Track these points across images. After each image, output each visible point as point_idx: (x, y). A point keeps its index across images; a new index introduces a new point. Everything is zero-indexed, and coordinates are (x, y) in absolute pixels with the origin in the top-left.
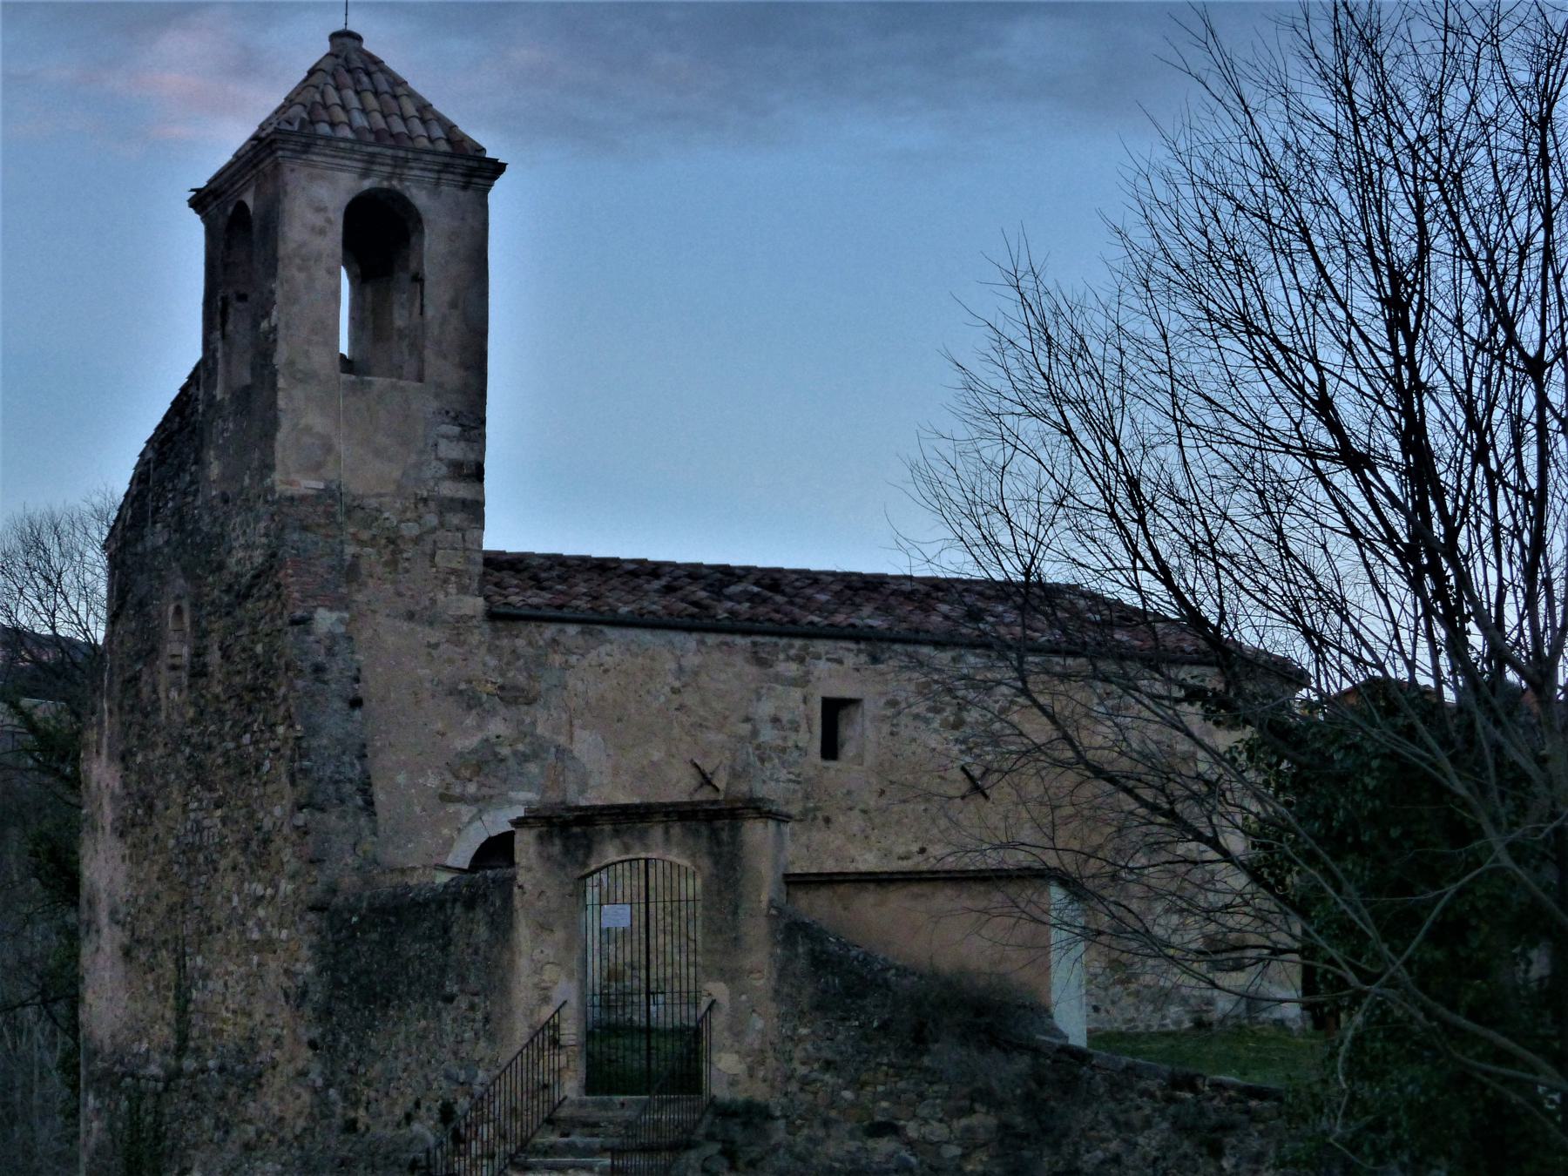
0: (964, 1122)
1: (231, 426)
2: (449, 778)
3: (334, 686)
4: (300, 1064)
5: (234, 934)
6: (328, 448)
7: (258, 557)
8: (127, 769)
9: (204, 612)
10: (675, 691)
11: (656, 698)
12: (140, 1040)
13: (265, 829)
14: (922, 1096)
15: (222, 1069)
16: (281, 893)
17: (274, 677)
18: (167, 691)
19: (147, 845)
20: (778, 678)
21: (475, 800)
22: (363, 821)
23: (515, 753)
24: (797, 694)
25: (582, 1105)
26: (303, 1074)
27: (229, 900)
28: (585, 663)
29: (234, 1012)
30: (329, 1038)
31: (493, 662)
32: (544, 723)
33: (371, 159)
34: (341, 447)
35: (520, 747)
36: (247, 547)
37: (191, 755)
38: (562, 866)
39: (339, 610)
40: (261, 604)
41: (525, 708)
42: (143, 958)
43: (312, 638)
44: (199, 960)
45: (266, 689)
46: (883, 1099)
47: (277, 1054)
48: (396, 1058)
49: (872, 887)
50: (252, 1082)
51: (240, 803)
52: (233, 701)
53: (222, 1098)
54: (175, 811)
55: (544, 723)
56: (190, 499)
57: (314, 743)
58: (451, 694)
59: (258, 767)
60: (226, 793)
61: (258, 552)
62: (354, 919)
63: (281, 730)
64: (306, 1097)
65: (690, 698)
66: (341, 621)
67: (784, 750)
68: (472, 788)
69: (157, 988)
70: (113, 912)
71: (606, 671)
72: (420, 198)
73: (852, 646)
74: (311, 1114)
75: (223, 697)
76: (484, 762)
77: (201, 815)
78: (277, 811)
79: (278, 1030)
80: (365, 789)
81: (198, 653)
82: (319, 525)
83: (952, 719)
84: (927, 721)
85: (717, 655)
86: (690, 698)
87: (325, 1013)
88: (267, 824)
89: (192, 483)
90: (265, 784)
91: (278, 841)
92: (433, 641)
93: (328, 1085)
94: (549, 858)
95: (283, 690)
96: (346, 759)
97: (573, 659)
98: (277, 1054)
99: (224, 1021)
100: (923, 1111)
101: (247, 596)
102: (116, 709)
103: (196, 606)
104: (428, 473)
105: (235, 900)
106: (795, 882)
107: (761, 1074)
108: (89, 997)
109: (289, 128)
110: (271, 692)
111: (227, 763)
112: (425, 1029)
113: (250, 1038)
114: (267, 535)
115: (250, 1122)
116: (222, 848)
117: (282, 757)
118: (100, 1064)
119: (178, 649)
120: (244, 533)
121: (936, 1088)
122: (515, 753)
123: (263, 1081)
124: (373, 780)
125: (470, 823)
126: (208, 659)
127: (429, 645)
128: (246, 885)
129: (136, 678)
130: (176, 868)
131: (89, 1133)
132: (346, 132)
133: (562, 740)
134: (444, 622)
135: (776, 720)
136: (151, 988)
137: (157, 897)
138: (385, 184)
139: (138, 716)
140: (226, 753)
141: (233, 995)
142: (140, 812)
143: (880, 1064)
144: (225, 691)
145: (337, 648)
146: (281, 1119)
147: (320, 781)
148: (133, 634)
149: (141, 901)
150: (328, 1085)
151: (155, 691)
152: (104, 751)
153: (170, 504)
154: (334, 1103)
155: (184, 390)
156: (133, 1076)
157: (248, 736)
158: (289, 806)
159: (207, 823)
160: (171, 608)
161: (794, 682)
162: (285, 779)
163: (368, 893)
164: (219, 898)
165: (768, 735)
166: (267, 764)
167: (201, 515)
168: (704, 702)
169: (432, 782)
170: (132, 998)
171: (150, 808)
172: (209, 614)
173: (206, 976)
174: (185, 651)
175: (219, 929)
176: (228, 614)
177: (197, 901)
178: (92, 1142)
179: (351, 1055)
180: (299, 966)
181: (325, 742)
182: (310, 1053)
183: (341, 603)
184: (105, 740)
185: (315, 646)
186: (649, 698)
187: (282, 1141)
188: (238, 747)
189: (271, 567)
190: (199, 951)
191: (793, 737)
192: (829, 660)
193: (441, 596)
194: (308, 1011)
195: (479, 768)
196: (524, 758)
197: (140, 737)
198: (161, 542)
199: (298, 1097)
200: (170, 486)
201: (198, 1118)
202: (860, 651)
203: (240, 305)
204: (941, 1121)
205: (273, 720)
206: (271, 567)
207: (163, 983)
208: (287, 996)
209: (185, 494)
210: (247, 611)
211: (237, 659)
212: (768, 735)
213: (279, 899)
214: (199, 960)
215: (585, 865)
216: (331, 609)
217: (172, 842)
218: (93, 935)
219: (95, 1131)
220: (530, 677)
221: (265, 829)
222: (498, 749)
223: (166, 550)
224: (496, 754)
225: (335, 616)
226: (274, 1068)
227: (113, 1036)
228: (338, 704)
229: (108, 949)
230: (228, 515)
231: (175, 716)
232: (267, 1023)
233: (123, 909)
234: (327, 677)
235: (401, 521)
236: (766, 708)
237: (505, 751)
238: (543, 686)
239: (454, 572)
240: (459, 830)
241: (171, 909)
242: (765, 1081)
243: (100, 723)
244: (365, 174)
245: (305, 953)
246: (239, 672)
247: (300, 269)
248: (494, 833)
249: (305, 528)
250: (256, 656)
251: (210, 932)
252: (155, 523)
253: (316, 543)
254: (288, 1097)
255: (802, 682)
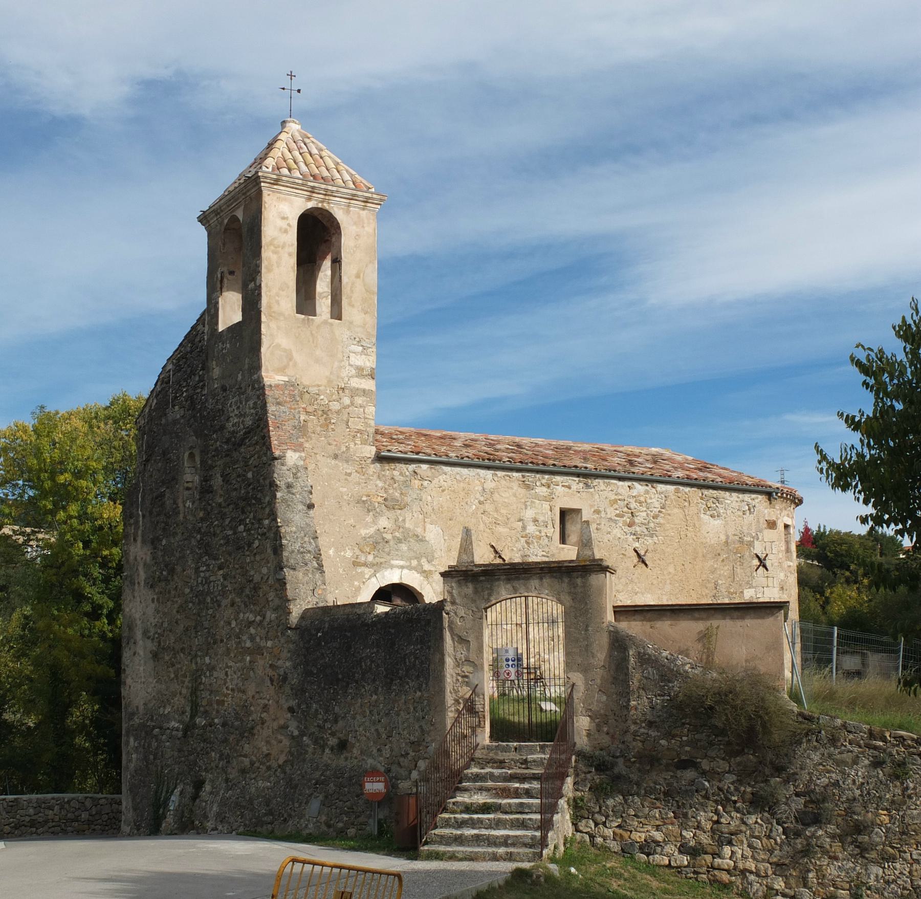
0: (738, 759)
1: (228, 345)
2: (358, 552)
3: (298, 496)
4: (282, 722)
5: (232, 644)
6: (290, 358)
7: (249, 421)
8: (155, 548)
9: (210, 455)
10: (480, 503)
11: (471, 507)
12: (164, 707)
13: (255, 581)
14: (711, 744)
15: (224, 725)
16: (268, 619)
17: (261, 491)
18: (184, 502)
19: (169, 592)
20: (537, 497)
21: (372, 565)
22: (318, 575)
23: (394, 537)
24: (546, 506)
25: (489, 748)
26: (285, 727)
27: (230, 624)
28: (432, 485)
29: (233, 690)
30: (303, 706)
31: (380, 484)
32: (410, 520)
33: (313, 190)
34: (297, 357)
35: (397, 534)
36: (240, 415)
37: (201, 539)
38: (474, 601)
39: (299, 451)
40: (252, 449)
41: (399, 511)
42: (167, 658)
43: (285, 468)
44: (207, 660)
45: (256, 499)
46: (687, 746)
47: (264, 715)
48: (398, 715)
49: (668, 614)
50: (248, 732)
51: (237, 566)
52: (231, 506)
53: (225, 741)
54: (190, 572)
55: (410, 520)
56: (199, 390)
57: (288, 530)
58: (358, 503)
59: (250, 544)
60: (227, 561)
61: (248, 419)
62: (319, 634)
63: (266, 522)
64: (286, 742)
65: (488, 507)
66: (301, 457)
67: (540, 538)
68: (370, 558)
69: (176, 676)
70: (145, 633)
71: (443, 491)
72: (339, 214)
73: (577, 479)
74: (290, 752)
75: (223, 504)
76: (378, 543)
77: (208, 574)
78: (265, 570)
79: (266, 702)
80: (318, 556)
81: (206, 479)
82: (286, 402)
83: (628, 520)
84: (615, 522)
85: (503, 482)
86: (488, 507)
87: (299, 692)
88: (257, 578)
89: (200, 381)
90: (255, 554)
91: (265, 588)
92: (348, 471)
93: (302, 734)
94: (466, 596)
95: (267, 499)
96: (306, 539)
97: (425, 483)
98: (264, 715)
99: (226, 695)
100: (712, 753)
101: (240, 445)
102: (148, 514)
103: (204, 452)
104: (344, 374)
105: (234, 624)
106: (622, 612)
107: (605, 729)
108: (129, 681)
109: (267, 170)
110: (259, 501)
111: (227, 543)
112: (376, 701)
113: (244, 706)
114: (254, 408)
115: (245, 756)
116: (224, 593)
117: (267, 538)
118: (137, 721)
119: (190, 477)
120: (238, 408)
121: (720, 738)
122: (394, 537)
123: (255, 731)
124: (322, 552)
125: (369, 579)
126: (212, 483)
127: (346, 474)
128: (241, 615)
129: (162, 495)
130: (191, 605)
131: (130, 761)
132: (297, 174)
133: (419, 531)
134: (355, 460)
135: (535, 521)
136: (172, 676)
137: (177, 622)
138: (320, 205)
139: (162, 518)
140: (226, 538)
141: (232, 680)
142: (164, 573)
143: (684, 724)
144: (225, 501)
145: (299, 474)
146: (268, 755)
147: (293, 552)
148: (159, 471)
149: (165, 625)
150: (302, 734)
151: (175, 503)
152: (139, 539)
153: (185, 394)
154: (308, 746)
155: (193, 328)
156: (161, 728)
157: (242, 527)
158: (273, 567)
159: (212, 578)
160: (187, 455)
161: (546, 499)
162: (269, 550)
163: (327, 619)
164: (222, 623)
165: (531, 529)
166: (257, 543)
167: (207, 400)
168: (497, 510)
169: (349, 554)
170: (159, 681)
171: (172, 571)
172: (214, 456)
173: (212, 668)
174: (197, 478)
175: (222, 641)
176: (227, 456)
177: (206, 624)
178: (132, 766)
179: (320, 717)
180: (280, 663)
181: (294, 529)
182: (289, 715)
183: (299, 448)
184: (140, 532)
185: (287, 472)
186: (467, 507)
187: (269, 768)
188: (235, 533)
189: (258, 426)
190: (207, 655)
191: (544, 530)
192: (563, 486)
193: (352, 445)
194: (287, 689)
195: (375, 545)
196: (399, 541)
197: (164, 529)
198: (178, 416)
199: (281, 742)
200: (185, 384)
201: (207, 753)
202: (580, 481)
203: (230, 277)
204: (723, 759)
205: (260, 517)
206: (258, 426)
207: (181, 673)
208: (272, 680)
209: (195, 388)
210: (241, 454)
211: (234, 482)
212: (531, 529)
213: (265, 623)
214: (207, 660)
215: (488, 600)
216: (295, 451)
217: (187, 590)
218: (131, 644)
219: (134, 760)
220: (402, 494)
221: (255, 581)
222: (385, 535)
223: (182, 421)
224: (383, 539)
225: (298, 454)
226: (263, 724)
227: (145, 704)
228: (301, 507)
229: (142, 653)
230: (226, 398)
231: (190, 517)
232: (257, 696)
233: (152, 631)
234: (294, 491)
235: (330, 401)
236: (529, 514)
237: (388, 536)
238: (408, 499)
239: (359, 431)
240: (364, 583)
241: (187, 629)
242: (608, 734)
243: (137, 522)
244: (309, 199)
245: (285, 654)
246: (236, 489)
247: (275, 252)
248: (383, 585)
249: (279, 404)
250: (248, 479)
251: (215, 643)
252: (173, 406)
253: (285, 412)
254: (274, 742)
255: (550, 498)
